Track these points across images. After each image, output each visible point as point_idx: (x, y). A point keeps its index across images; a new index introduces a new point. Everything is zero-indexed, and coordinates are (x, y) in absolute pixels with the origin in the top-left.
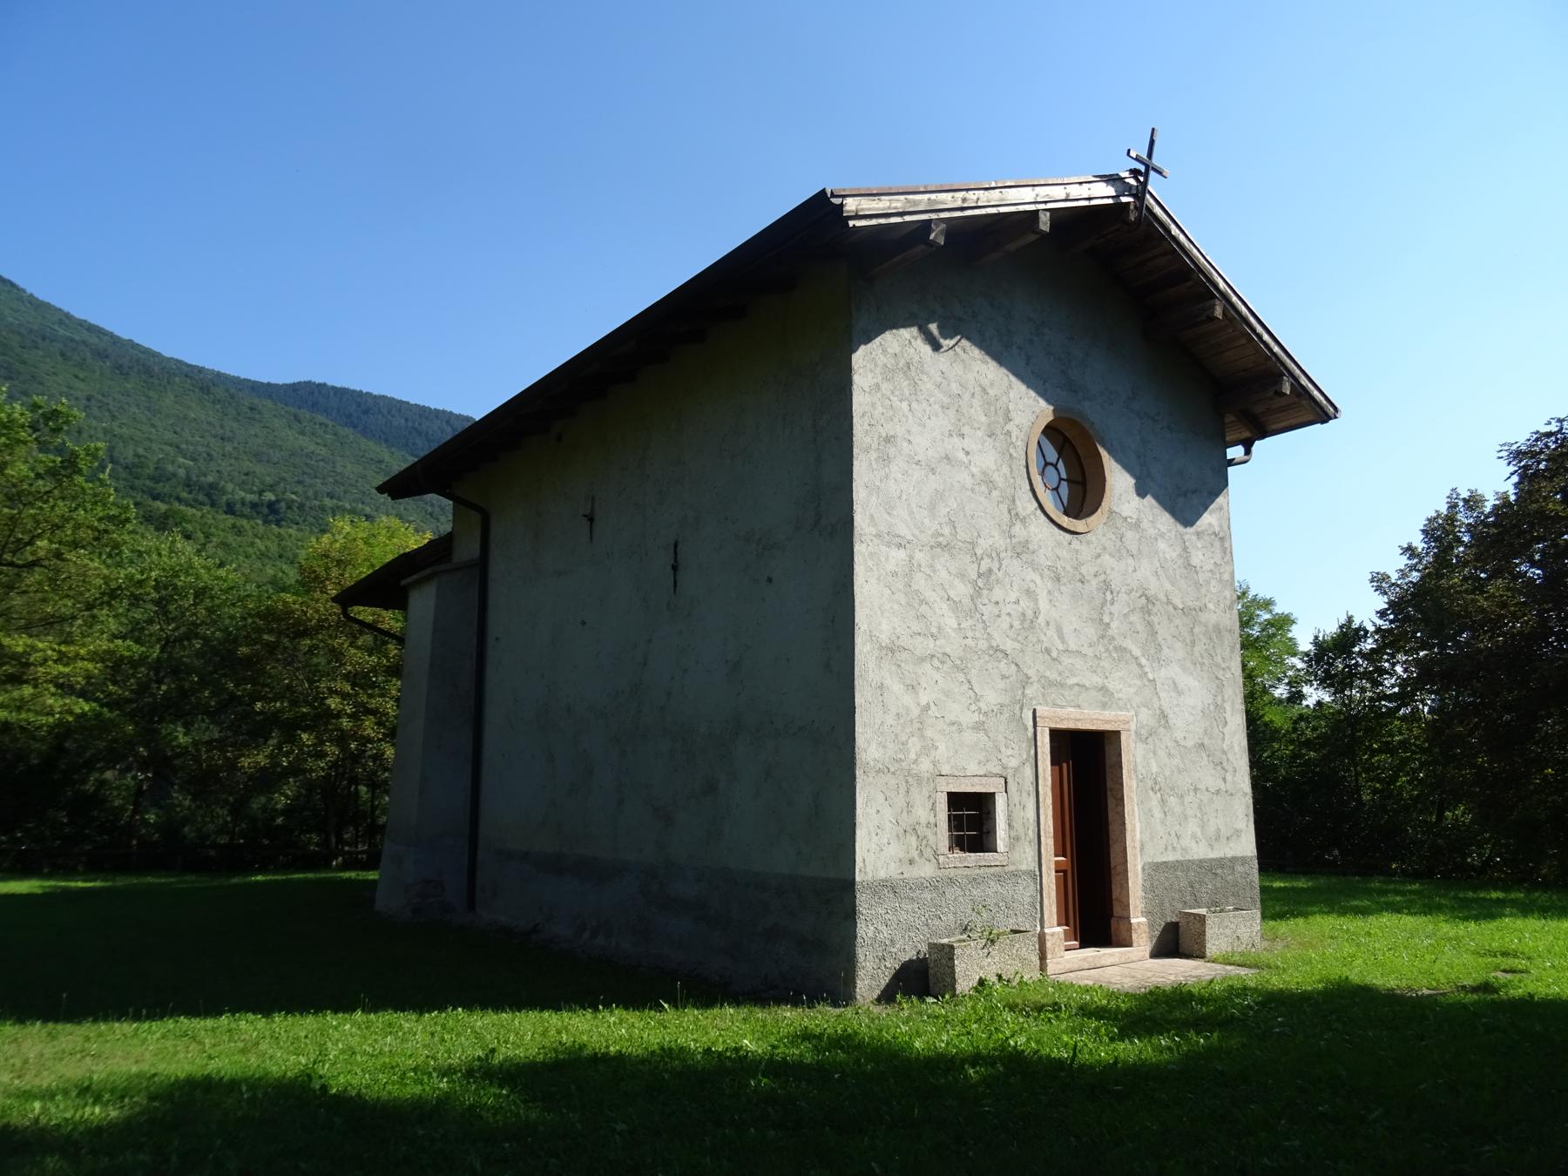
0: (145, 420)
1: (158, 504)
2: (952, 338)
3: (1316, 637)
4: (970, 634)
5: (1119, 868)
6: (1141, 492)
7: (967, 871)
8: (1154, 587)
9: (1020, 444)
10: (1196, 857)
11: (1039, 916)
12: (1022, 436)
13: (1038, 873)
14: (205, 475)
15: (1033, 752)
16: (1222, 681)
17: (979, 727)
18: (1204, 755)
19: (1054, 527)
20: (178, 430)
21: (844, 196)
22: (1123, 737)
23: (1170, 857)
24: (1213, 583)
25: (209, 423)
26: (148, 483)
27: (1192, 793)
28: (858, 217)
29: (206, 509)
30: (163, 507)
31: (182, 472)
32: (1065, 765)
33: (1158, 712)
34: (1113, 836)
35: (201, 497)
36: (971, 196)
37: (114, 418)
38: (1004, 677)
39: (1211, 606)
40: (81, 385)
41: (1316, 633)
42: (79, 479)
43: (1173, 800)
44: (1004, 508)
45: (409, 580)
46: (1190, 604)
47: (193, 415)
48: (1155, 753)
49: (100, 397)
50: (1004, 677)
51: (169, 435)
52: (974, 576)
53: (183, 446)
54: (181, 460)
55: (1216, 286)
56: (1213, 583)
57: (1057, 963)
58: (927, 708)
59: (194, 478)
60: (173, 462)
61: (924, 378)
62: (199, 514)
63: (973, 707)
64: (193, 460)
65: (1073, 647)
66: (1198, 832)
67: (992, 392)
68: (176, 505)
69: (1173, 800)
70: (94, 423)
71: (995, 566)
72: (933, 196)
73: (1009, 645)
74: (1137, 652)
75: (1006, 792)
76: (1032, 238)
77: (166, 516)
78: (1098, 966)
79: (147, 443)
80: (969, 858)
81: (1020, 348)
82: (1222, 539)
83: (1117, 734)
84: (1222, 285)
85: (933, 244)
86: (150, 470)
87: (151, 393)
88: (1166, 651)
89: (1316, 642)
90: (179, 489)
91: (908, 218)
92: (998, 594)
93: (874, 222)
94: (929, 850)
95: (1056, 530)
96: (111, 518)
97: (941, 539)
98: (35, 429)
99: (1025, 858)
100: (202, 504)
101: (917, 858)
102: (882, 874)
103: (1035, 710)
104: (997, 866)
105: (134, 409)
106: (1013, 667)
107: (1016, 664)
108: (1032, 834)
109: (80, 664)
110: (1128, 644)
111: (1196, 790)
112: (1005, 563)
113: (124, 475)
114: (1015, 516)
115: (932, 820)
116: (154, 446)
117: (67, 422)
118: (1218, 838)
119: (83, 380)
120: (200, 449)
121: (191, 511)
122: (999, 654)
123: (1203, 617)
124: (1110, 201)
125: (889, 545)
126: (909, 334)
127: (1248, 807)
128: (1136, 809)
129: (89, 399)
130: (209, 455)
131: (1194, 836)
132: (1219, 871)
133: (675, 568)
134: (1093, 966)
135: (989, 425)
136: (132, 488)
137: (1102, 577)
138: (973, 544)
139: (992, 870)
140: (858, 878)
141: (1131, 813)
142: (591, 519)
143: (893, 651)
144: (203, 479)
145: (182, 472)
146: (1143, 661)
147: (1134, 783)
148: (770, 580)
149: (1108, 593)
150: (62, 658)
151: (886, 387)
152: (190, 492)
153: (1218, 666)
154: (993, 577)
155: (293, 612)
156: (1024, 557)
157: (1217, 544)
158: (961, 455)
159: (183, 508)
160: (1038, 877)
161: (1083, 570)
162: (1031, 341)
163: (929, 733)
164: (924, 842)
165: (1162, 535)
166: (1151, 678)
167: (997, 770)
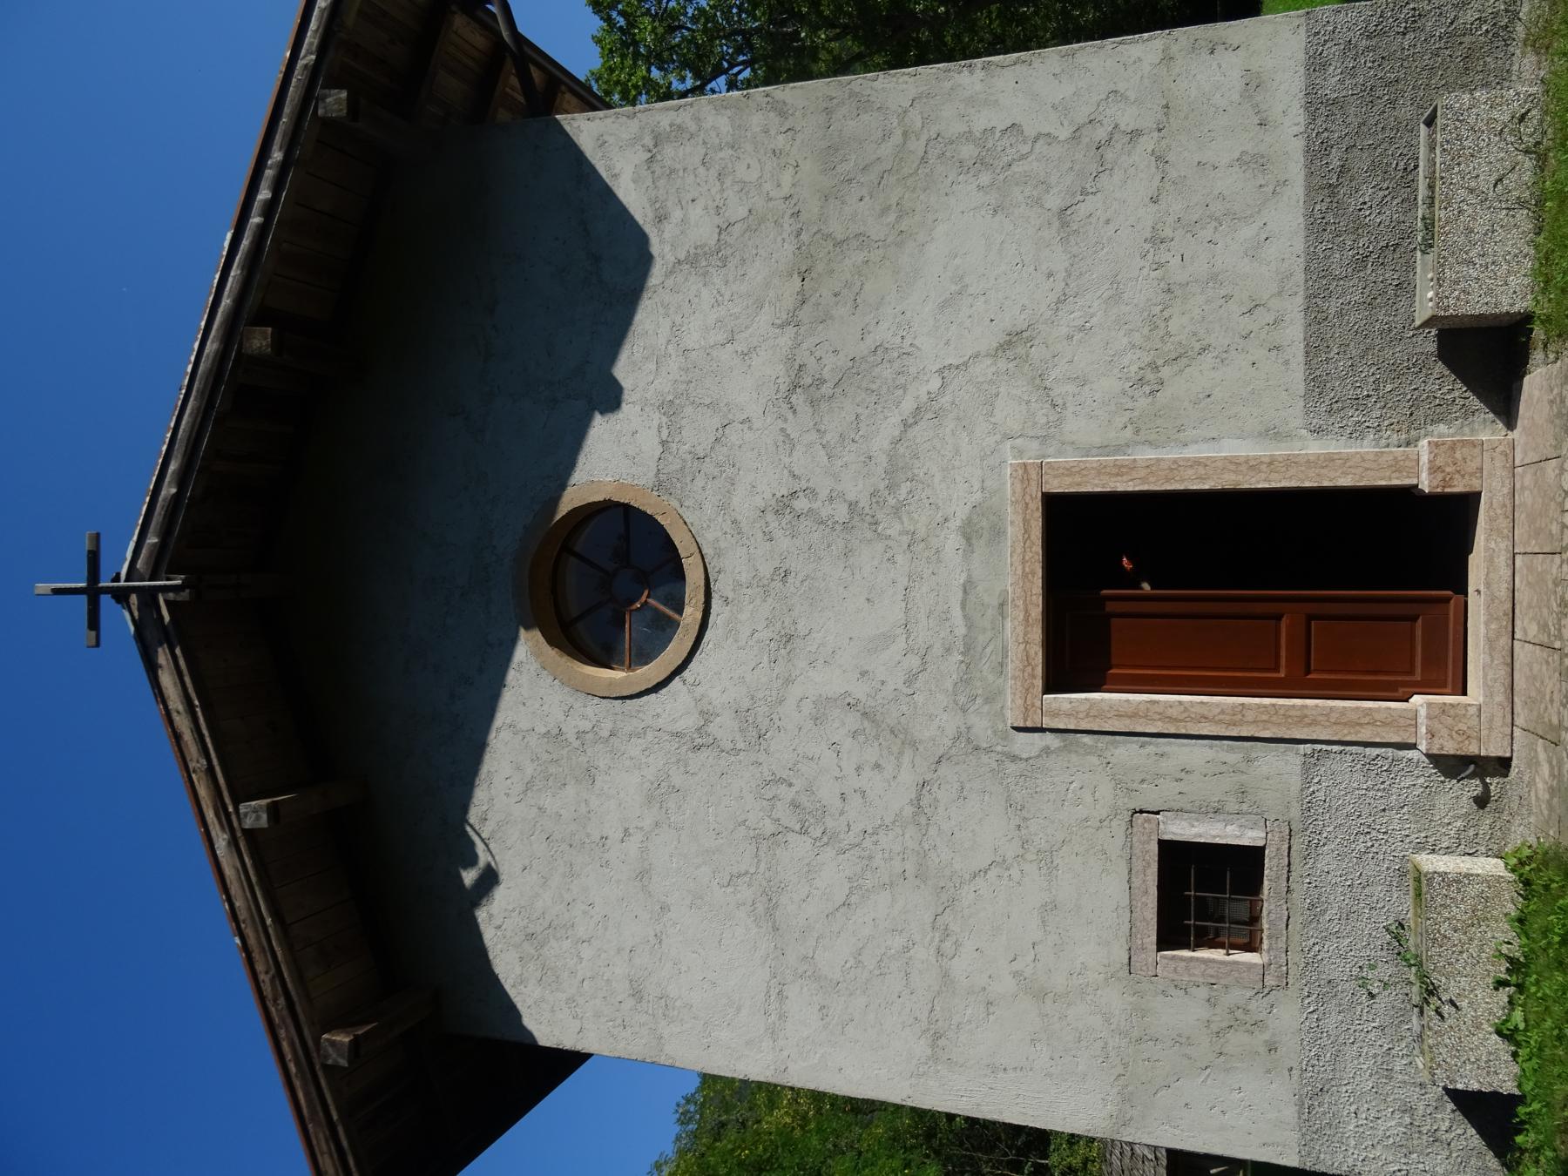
2: (472, 844)
9: (595, 708)
10: (1299, 246)
11: (1390, 752)
13: (1308, 748)
15: (1086, 739)
16: (929, 141)
18: (1083, 210)
19: (705, 640)
22: (1057, 486)
23: (1294, 333)
55: (222, 356)
57: (1491, 720)
75: (1157, 813)
78: (1509, 605)
80: (1273, 916)
84: (212, 347)
94: (1253, 1005)
95: (708, 635)
101: (1266, 1036)
102: (1290, 1112)
103: (1013, 728)
104: (1290, 848)
107: (939, 762)
115: (1203, 992)
122: (924, 803)
134: (1506, 622)
138: (758, 838)
141: (1201, 470)
164: (1239, 1014)
166: (935, 383)
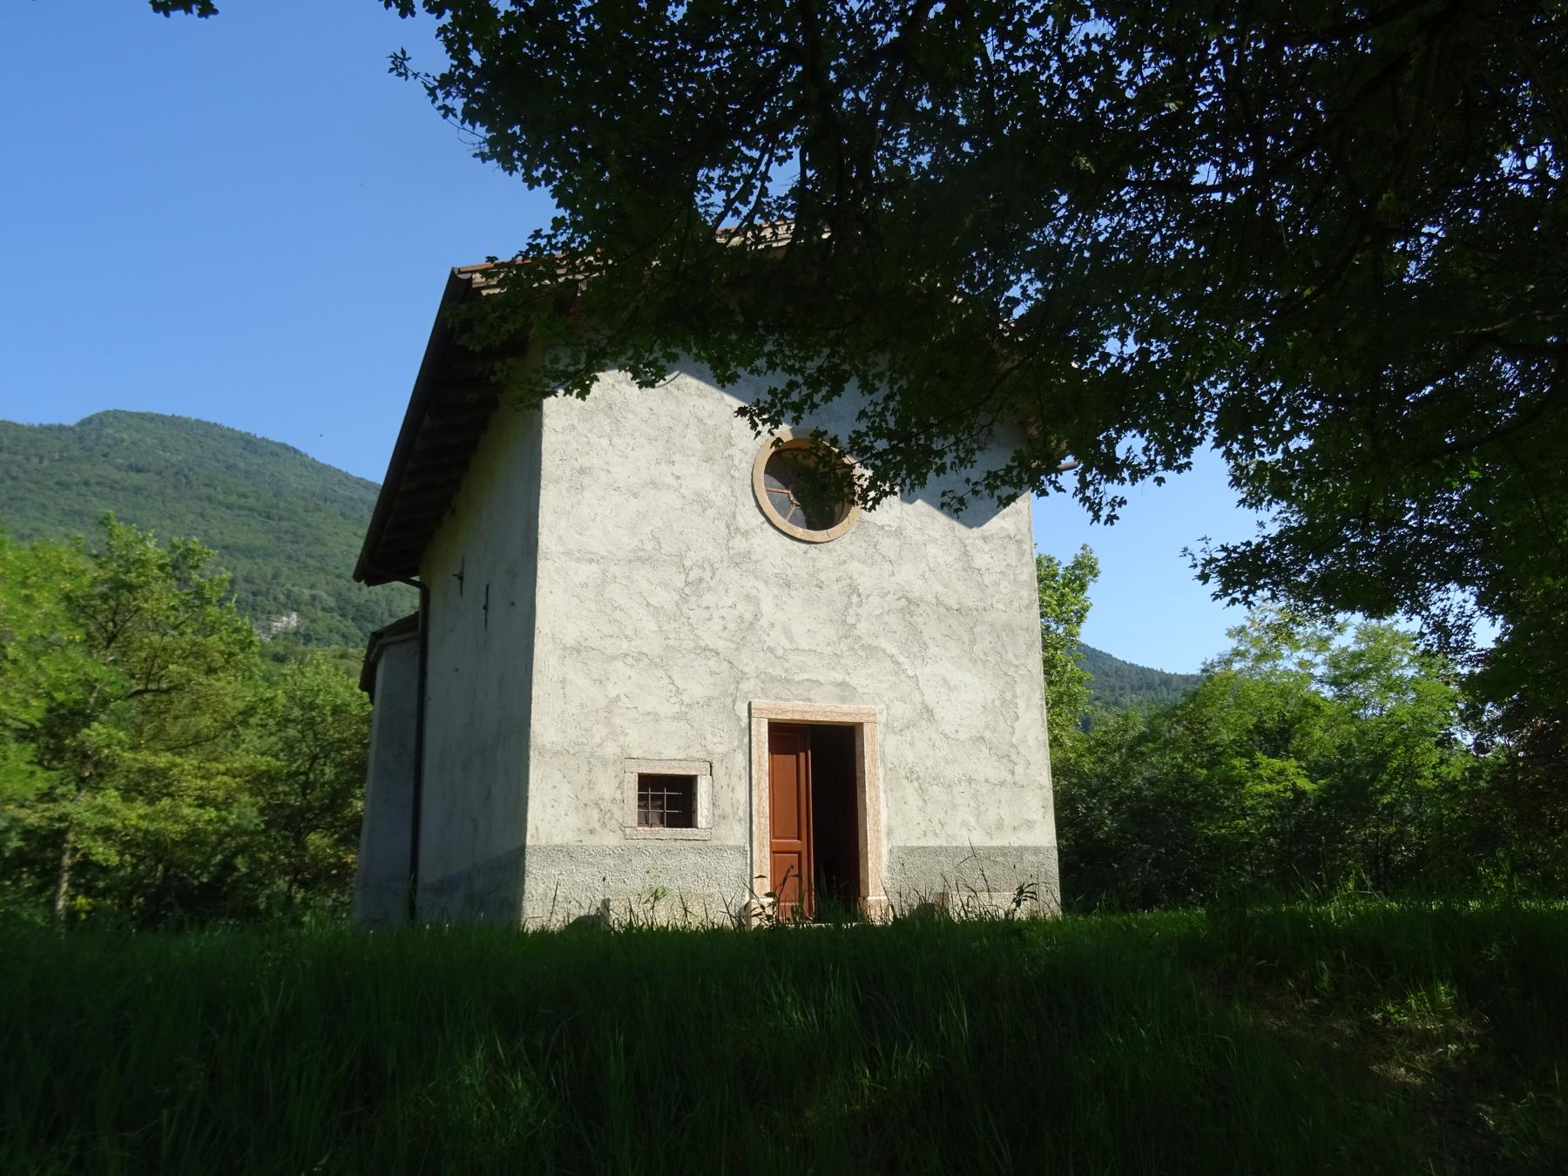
4: (672, 636)
5: (864, 851)
8: (918, 588)
15: (746, 740)
17: (679, 717)
22: (866, 729)
24: (1004, 583)
33: (919, 706)
34: (860, 823)
38: (712, 673)
44: (721, 525)
46: (971, 604)
48: (912, 744)
50: (712, 673)
58: (618, 698)
61: (630, 416)
63: (674, 700)
65: (803, 645)
66: (973, 821)
73: (720, 645)
74: (891, 649)
82: (1019, 542)
83: (861, 724)
88: (933, 649)
92: (709, 599)
97: (641, 554)
99: (735, 834)
102: (557, 840)
106: (726, 664)
109: (219, 778)
110: (883, 643)
112: (718, 573)
114: (732, 529)
123: (988, 617)
125: (579, 560)
127: (1045, 799)
128: (882, 795)
131: (964, 824)
133: (485, 608)
137: (848, 581)
138: (681, 557)
139: (692, 843)
140: (529, 842)
142: (461, 578)
143: (578, 651)
146: (901, 659)
153: (1008, 663)
154: (704, 585)
156: (744, 566)
157: (1012, 547)
158: (670, 480)
161: (822, 576)
163: (617, 721)
165: (935, 541)
167: (702, 755)
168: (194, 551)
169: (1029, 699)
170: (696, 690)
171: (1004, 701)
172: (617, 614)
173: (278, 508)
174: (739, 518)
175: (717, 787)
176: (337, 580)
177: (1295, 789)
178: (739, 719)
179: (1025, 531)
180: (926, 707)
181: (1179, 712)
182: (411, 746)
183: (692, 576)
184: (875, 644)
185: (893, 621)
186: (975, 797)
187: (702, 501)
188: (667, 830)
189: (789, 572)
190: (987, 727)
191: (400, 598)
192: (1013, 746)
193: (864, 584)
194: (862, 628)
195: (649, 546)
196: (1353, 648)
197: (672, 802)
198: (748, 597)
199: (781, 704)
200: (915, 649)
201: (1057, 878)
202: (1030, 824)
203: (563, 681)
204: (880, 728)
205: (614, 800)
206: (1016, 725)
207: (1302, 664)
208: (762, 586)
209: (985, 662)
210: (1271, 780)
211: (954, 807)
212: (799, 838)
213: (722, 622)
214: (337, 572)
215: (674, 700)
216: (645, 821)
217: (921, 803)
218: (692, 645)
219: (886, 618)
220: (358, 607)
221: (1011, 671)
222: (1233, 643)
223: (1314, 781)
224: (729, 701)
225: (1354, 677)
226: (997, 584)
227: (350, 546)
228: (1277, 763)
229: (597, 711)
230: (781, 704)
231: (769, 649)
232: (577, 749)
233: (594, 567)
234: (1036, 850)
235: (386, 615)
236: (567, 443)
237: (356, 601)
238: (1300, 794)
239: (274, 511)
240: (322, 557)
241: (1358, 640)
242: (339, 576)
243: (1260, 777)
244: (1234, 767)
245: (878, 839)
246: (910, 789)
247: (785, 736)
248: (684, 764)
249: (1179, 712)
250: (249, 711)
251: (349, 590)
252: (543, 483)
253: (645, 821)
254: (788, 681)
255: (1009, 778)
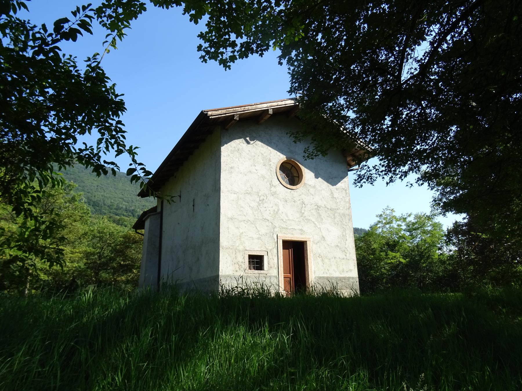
0: (113, 191)
1: (117, 216)
3: (448, 229)
4: (256, 215)
5: (307, 278)
6: (317, 177)
7: (254, 275)
8: (320, 203)
12: (275, 165)
14: (131, 207)
15: (277, 245)
17: (259, 238)
20: (123, 193)
21: (208, 112)
22: (308, 243)
24: (342, 202)
25: (132, 191)
26: (114, 210)
27: (333, 259)
28: (212, 116)
29: (131, 217)
30: (118, 217)
31: (124, 207)
32: (290, 250)
33: (321, 236)
34: (306, 269)
35: (130, 214)
36: (246, 107)
37: (105, 191)
38: (267, 226)
39: (341, 208)
40: (95, 182)
41: (447, 227)
42: (76, 203)
43: (326, 260)
44: (268, 184)
45: (145, 218)
46: (333, 208)
47: (127, 189)
48: (320, 247)
49: (101, 186)
50: (267, 226)
51: (120, 196)
52: (258, 200)
53: (125, 199)
54: (124, 203)
56: (342, 202)
58: (243, 233)
59: (128, 208)
60: (122, 204)
61: (243, 152)
62: (129, 219)
63: (257, 233)
64: (128, 203)
65: (291, 218)
66: (336, 269)
67: (265, 155)
68: (123, 217)
69: (326, 260)
70: (99, 193)
71: (265, 198)
72: (234, 109)
73: (269, 218)
74: (314, 220)
76: (269, 116)
77: (119, 220)
79: (114, 199)
81: (274, 143)
82: (346, 190)
83: (306, 241)
85: (236, 120)
86: (115, 207)
87: (115, 183)
88: (324, 220)
89: (448, 229)
90: (123, 212)
91: (227, 115)
92: (265, 205)
93: (217, 116)
96: (85, 213)
97: (247, 192)
98: (65, 190)
99: (274, 272)
100: (130, 216)
102: (227, 274)
105: (111, 188)
106: (271, 224)
108: (276, 266)
109: (76, 254)
110: (311, 218)
111: (335, 258)
112: (268, 197)
113: (108, 209)
114: (271, 185)
116: (116, 199)
117: (73, 187)
118: (343, 271)
119: (96, 181)
120: (130, 199)
121: (126, 218)
123: (338, 211)
124: (293, 104)
125: (231, 193)
126: (242, 140)
127: (355, 263)
128: (312, 261)
129: (97, 186)
130: (132, 201)
131: (334, 270)
132: (343, 280)
133: (193, 206)
135: (264, 163)
136: (110, 212)
137: (302, 201)
138: (258, 193)
139: (263, 275)
140: (220, 274)
142: (180, 197)
143: (232, 219)
144: (130, 208)
145: (124, 207)
146: (316, 223)
147: (312, 255)
148: (208, 205)
149: (304, 205)
150: (72, 253)
151: (231, 155)
152: (127, 213)
153: (343, 224)
154: (264, 201)
155: (132, 236)
156: (275, 196)
157: (344, 191)
158: (255, 171)
159: (124, 217)
160: (278, 278)
161: (295, 199)
162: (278, 141)
163: (242, 239)
165: (324, 189)
167: (265, 249)
168: (71, 185)
169: (349, 235)
170: (263, 231)
171: (343, 235)
172: (242, 209)
173: (70, 171)
174: (273, 182)
175: (269, 259)
176: (88, 194)
177: (399, 261)
178: (274, 239)
179: (347, 187)
180: (323, 237)
181: (363, 239)
182: (157, 245)
183: (261, 198)
184: (309, 218)
185: (314, 212)
186: (336, 262)
187: (264, 177)
188: (256, 271)
189: (286, 197)
190: (339, 243)
191: (151, 202)
192: (346, 248)
193: (306, 202)
194: (306, 214)
195: (250, 189)
196: (413, 221)
197: (257, 263)
198: (276, 204)
199: (285, 235)
200: (319, 220)
201: (358, 286)
202: (351, 270)
203: (228, 228)
204: (312, 242)
205: (242, 262)
206: (346, 242)
207: (398, 225)
208: (279, 201)
209: (338, 224)
210: (392, 259)
211: (331, 265)
212: (290, 274)
213: (269, 212)
214: (88, 191)
215: (257, 233)
216: (250, 268)
217: (322, 264)
218: (261, 218)
219: (312, 211)
220: (94, 202)
221: (345, 227)
222: (378, 219)
223: (405, 259)
224: (272, 234)
225: (415, 229)
226: (340, 202)
227: (92, 183)
228: (394, 254)
229: (237, 236)
230: (285, 235)
231: (282, 219)
232: (232, 247)
233: (235, 195)
234: (353, 278)
235: (103, 205)
236: (227, 160)
237: (94, 200)
238: (401, 263)
239: (69, 172)
240: (83, 186)
241: (415, 219)
242: (88, 192)
243: (389, 258)
244: (381, 255)
245: (312, 274)
246: (319, 260)
247: (287, 244)
248: (260, 252)
249: (363, 239)
250: (86, 234)
251: (91, 197)
252: (221, 171)
253: (250, 268)
254: (287, 229)
255: (345, 257)
